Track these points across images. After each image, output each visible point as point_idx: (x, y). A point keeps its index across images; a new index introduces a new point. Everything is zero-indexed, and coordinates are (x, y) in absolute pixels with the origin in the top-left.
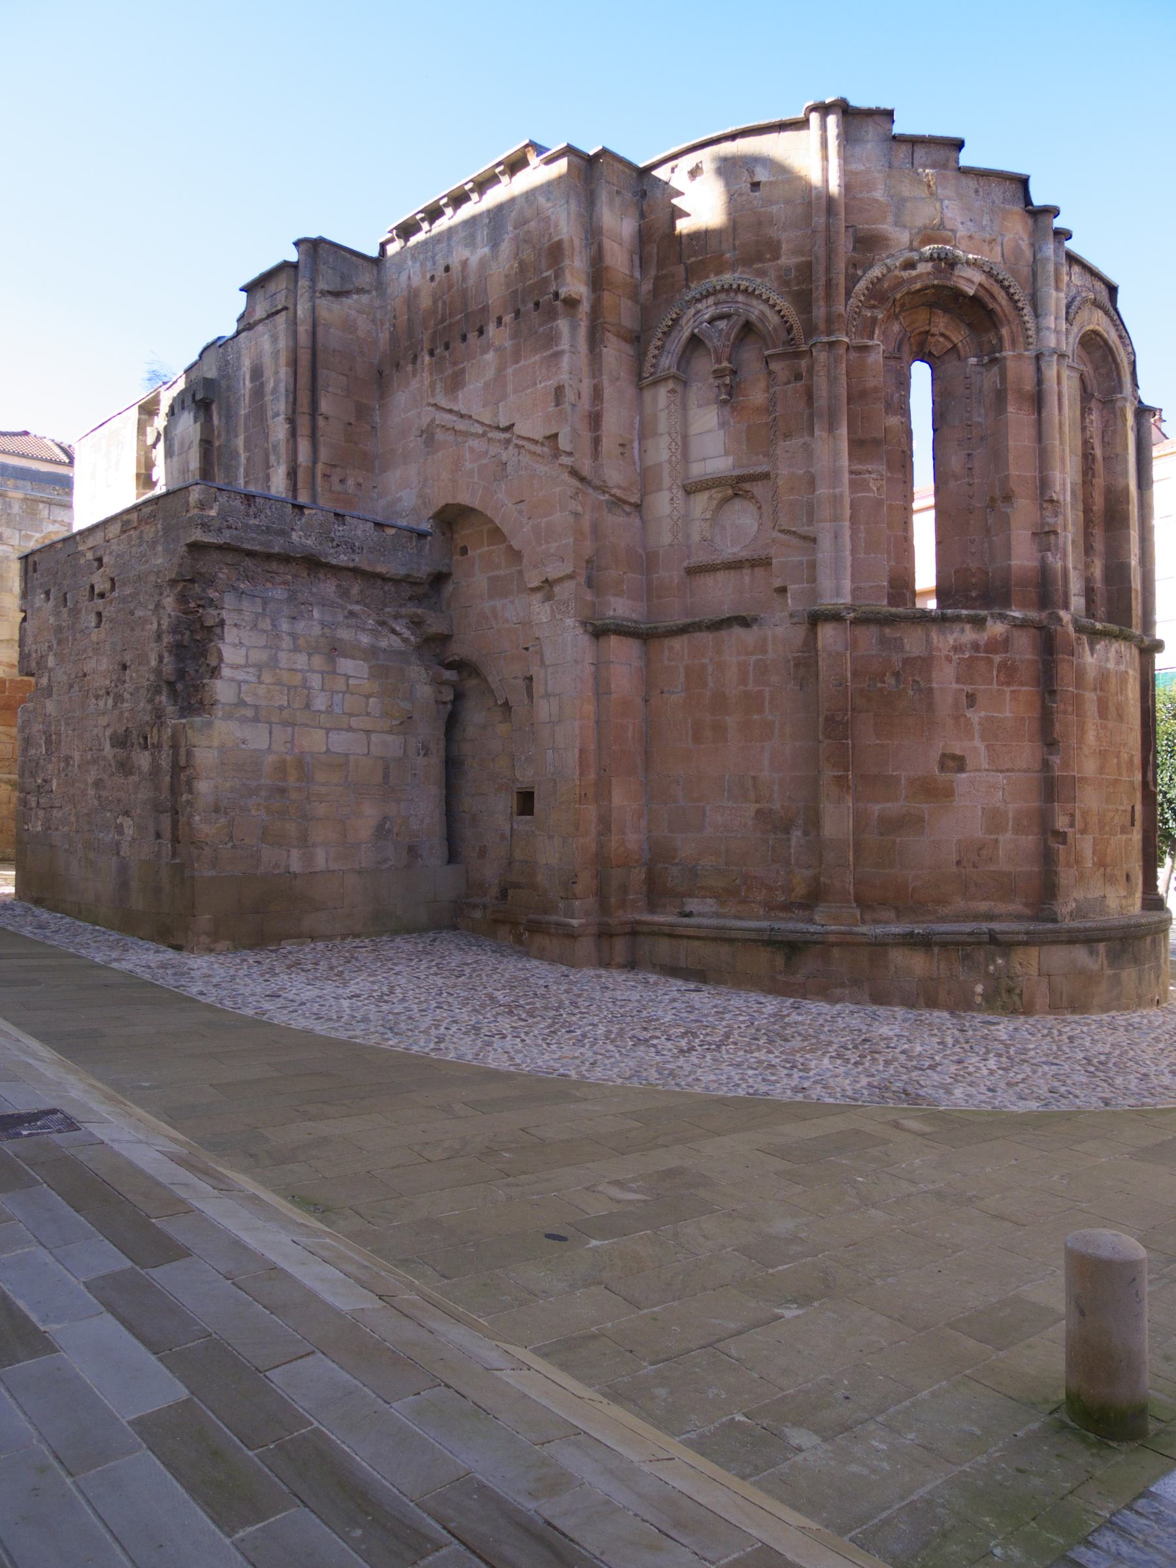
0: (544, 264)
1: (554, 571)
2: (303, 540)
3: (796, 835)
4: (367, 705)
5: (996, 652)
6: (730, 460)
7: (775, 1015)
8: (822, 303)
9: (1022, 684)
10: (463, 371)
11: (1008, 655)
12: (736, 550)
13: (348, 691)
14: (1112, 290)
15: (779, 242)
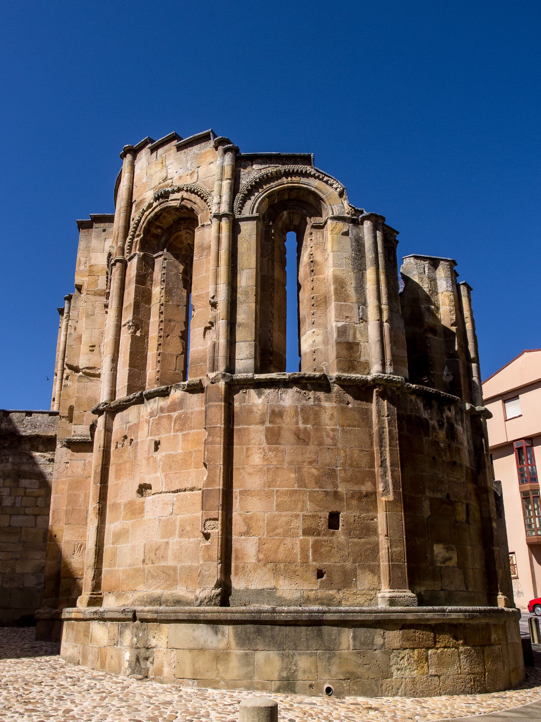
2: (7, 426)
4: (36, 501)
5: (174, 410)
11: (182, 411)
13: (25, 495)
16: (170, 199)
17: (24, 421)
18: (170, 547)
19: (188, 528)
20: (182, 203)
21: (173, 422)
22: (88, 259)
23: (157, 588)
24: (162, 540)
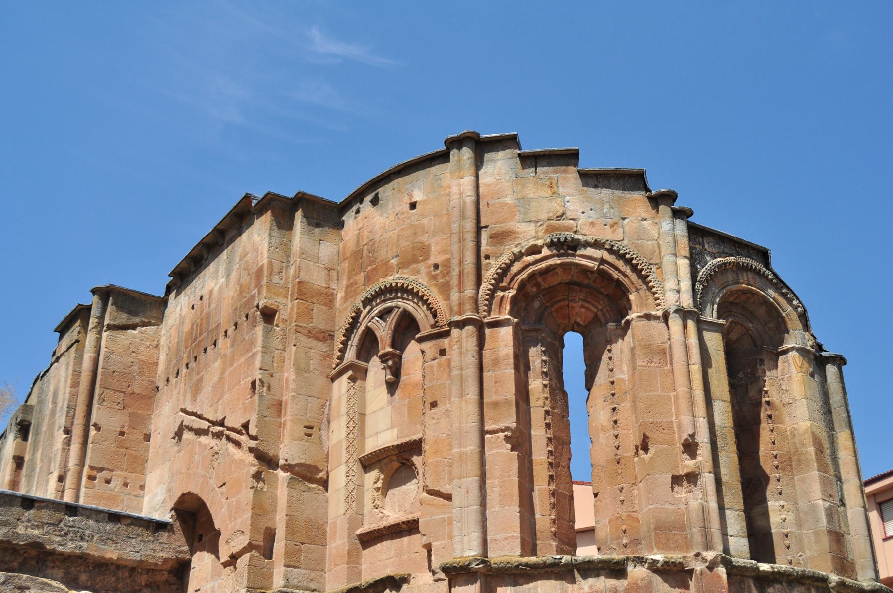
6: (395, 431)
8: (456, 289)
10: (202, 378)
15: (429, 246)
16: (578, 253)
17: (61, 525)
20: (602, 267)
22: (284, 265)
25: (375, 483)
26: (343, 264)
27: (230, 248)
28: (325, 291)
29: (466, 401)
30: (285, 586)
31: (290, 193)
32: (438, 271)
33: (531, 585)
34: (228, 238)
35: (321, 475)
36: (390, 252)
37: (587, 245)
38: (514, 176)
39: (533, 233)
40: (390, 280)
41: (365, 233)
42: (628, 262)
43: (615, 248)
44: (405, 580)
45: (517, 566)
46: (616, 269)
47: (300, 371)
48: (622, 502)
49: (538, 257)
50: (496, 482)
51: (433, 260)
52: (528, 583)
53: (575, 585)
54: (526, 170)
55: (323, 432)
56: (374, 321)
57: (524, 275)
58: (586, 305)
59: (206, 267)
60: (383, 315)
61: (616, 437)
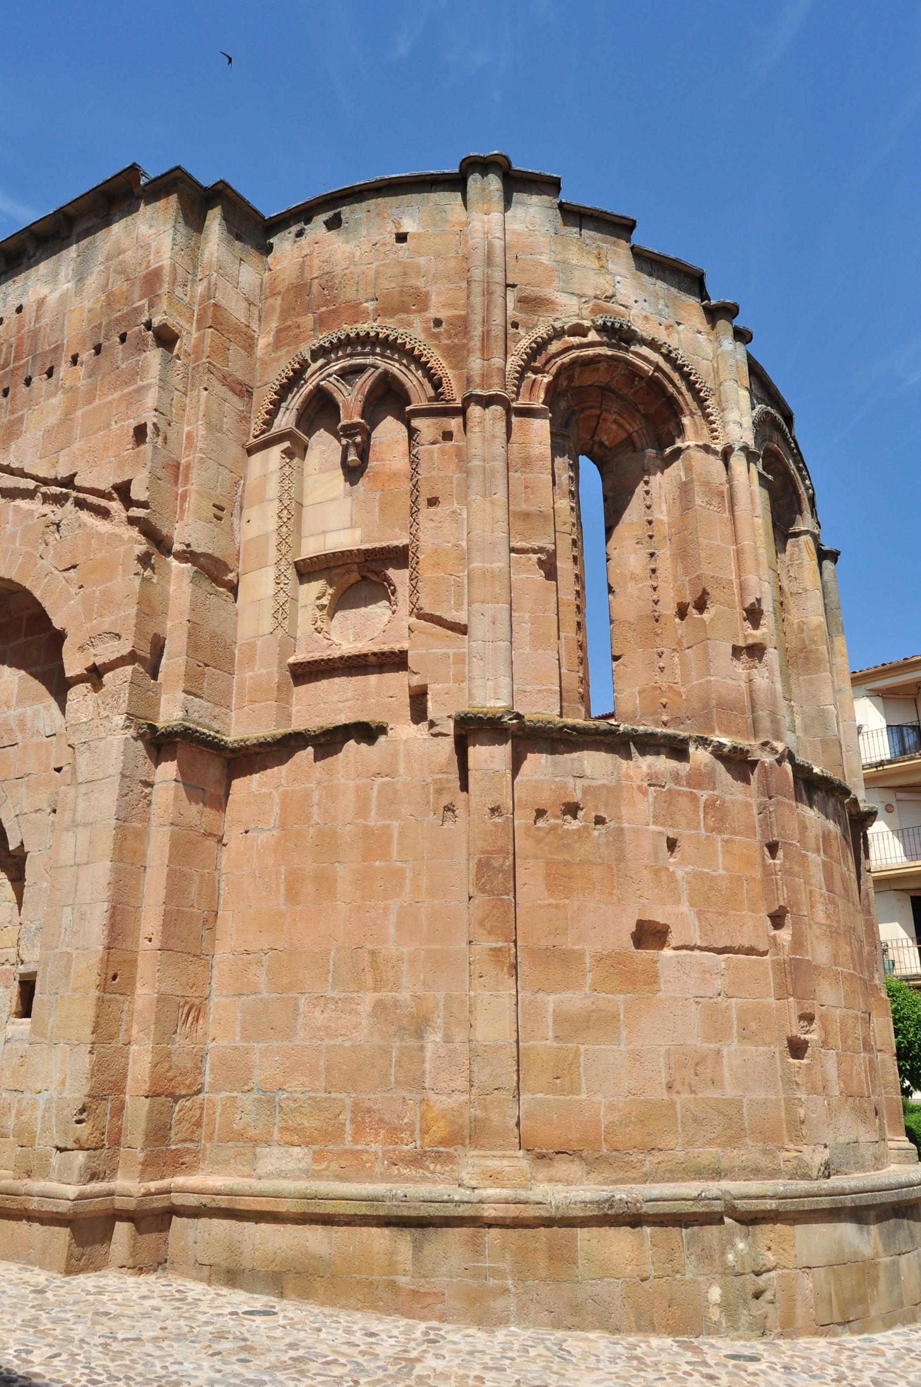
0: (137, 293)
1: (105, 653)
3: (433, 1039)
5: (699, 786)
6: (358, 533)
7: (397, 1360)
8: (478, 354)
9: (734, 832)
10: (21, 419)
11: (716, 793)
12: (359, 645)
14: (789, 418)
15: (427, 294)
16: (632, 348)
18: (725, 1060)
19: (753, 1026)
20: (656, 374)
21: (701, 809)
23: (708, 1144)
24: (706, 1045)
25: (319, 598)
26: (271, 301)
27: (85, 242)
28: (245, 329)
29: (492, 504)
30: (184, 720)
31: (207, 180)
32: (442, 329)
33: (575, 755)
34: (79, 228)
35: (231, 576)
36: (361, 292)
37: (643, 342)
38: (552, 231)
39: (576, 309)
40: (363, 327)
41: (316, 262)
42: (685, 376)
43: (673, 355)
44: (382, 730)
45: (561, 728)
46: (671, 381)
47: (213, 428)
48: (662, 669)
49: (585, 340)
50: (527, 616)
51: (432, 313)
52: (571, 752)
53: (630, 762)
54: (569, 229)
55: (235, 520)
56: (331, 379)
57: (566, 359)
58: (621, 420)
59: (30, 267)
60: (348, 374)
61: (655, 589)
